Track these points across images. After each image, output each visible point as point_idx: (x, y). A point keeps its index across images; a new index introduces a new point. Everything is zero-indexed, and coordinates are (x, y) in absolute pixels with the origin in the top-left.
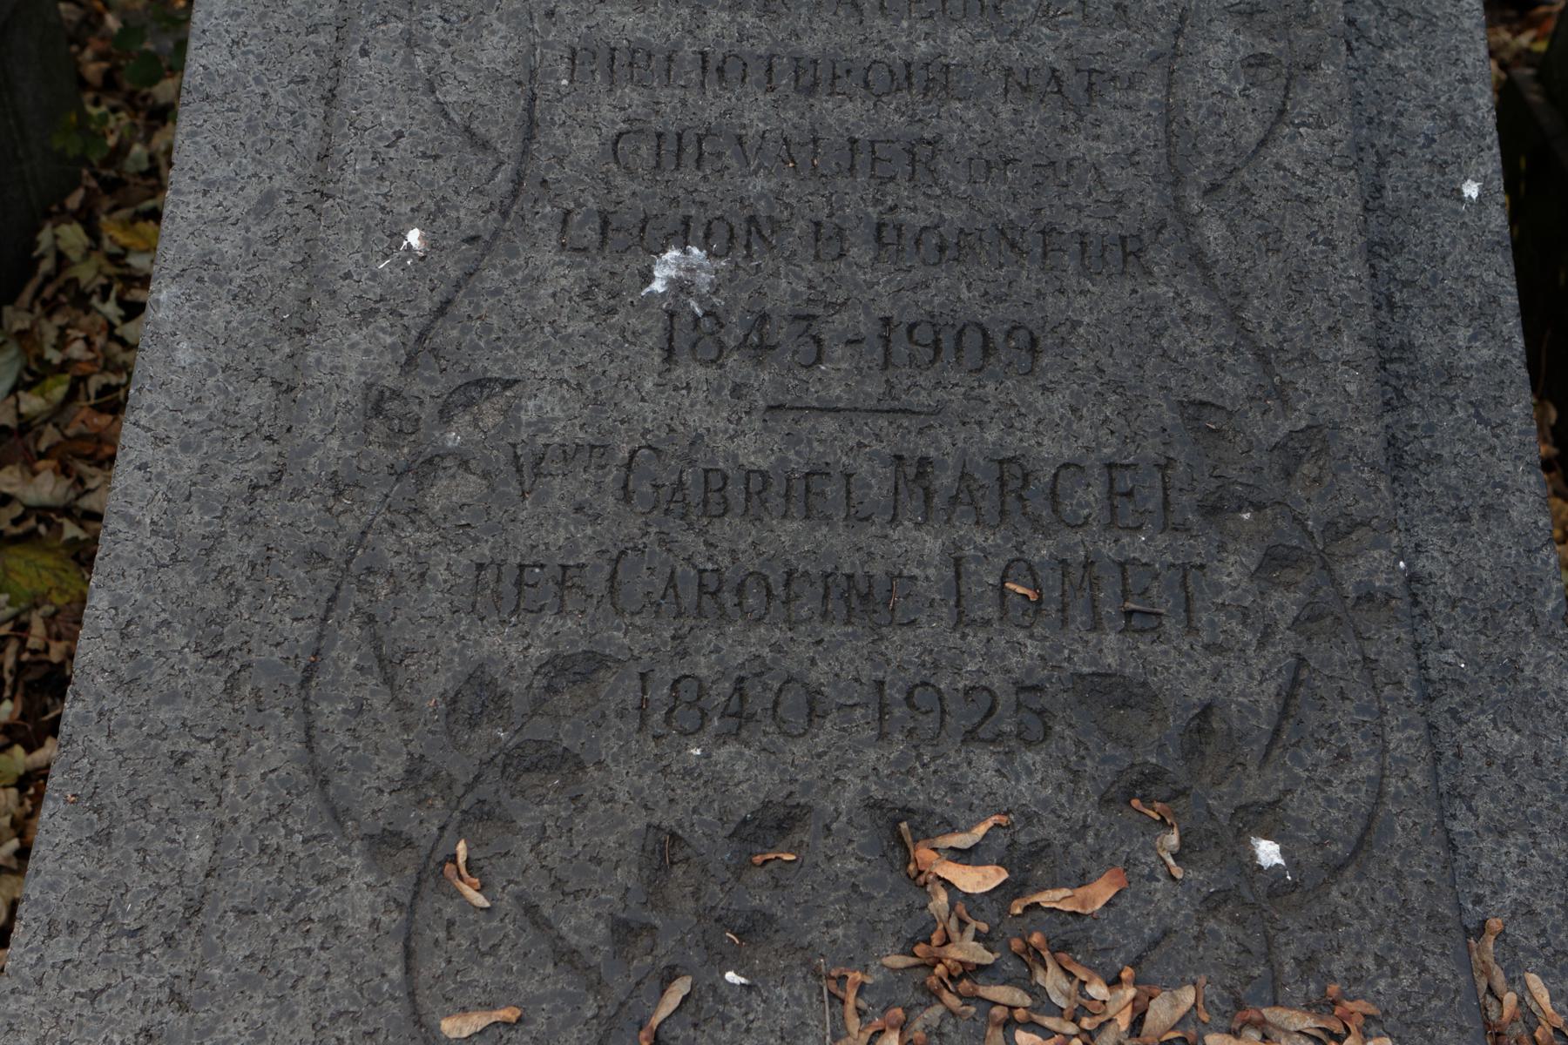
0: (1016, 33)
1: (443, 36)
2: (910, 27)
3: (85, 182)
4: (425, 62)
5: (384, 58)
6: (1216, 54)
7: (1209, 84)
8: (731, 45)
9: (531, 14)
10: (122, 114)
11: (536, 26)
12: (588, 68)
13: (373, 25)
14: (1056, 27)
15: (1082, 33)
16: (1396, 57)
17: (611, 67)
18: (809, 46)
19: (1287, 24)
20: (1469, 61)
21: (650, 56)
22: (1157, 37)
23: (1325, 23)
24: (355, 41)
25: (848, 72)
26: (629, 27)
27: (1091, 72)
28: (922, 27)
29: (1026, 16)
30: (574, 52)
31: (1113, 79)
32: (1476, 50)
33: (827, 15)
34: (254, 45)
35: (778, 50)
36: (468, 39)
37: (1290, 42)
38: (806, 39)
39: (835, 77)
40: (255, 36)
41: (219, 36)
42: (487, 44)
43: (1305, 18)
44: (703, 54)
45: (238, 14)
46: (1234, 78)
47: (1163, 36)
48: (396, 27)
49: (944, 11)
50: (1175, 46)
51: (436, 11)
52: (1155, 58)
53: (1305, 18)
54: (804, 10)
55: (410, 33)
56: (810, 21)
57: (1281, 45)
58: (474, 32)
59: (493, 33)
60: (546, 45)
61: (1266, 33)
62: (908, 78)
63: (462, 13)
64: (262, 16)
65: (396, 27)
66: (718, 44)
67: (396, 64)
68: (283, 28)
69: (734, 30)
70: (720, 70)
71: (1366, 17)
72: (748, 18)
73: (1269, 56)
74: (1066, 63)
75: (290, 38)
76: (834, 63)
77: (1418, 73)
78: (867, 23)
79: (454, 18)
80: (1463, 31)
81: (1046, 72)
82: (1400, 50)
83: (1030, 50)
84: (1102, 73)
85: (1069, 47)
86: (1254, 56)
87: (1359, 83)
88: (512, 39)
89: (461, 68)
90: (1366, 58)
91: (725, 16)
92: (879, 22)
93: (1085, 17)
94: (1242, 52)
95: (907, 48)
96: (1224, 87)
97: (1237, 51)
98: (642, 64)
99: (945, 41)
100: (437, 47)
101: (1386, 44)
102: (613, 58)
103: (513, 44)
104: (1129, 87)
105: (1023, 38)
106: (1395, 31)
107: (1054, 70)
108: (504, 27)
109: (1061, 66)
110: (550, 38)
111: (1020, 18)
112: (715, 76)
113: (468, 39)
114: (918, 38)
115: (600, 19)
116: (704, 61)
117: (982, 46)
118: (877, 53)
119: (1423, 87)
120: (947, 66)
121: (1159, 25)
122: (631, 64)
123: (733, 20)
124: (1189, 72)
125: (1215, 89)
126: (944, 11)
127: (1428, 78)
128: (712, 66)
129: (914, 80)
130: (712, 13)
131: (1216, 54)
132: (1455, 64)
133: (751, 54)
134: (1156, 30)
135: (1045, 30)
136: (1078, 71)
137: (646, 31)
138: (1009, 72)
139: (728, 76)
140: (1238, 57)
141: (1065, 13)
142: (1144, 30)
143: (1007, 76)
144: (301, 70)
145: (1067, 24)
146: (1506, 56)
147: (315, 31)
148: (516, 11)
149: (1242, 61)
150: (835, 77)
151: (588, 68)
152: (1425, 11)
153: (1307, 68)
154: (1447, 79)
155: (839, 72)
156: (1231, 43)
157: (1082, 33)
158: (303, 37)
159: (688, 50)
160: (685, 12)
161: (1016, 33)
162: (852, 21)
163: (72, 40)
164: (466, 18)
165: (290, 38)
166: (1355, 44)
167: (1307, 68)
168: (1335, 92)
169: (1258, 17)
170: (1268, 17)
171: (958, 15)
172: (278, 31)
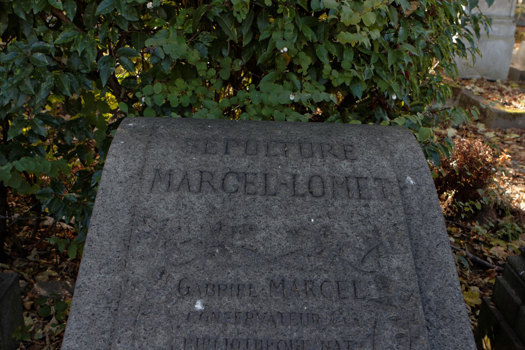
0: (324, 329)
1: (144, 335)
2: (291, 328)
3: (20, 346)
4: (138, 345)
5: (125, 344)
6: (387, 334)
7: (386, 345)
8: (235, 336)
9: (172, 327)
10: (36, 319)
11: (174, 331)
12: (190, 345)
13: (122, 332)
14: (337, 327)
15: (345, 328)
16: (443, 332)
17: (197, 344)
18: (260, 336)
19: (408, 323)
20: (466, 332)
21: (209, 341)
22: (368, 329)
23: (420, 323)
24: (116, 338)
25: (272, 344)
26: (203, 331)
27: (349, 341)
28: (295, 328)
29: (327, 323)
30: (185, 340)
31: (356, 344)
32: (468, 329)
33: (265, 325)
34: (84, 339)
35: (250, 337)
36: (152, 336)
37: (410, 329)
38: (258, 333)
39: (268, 346)
40: (85, 335)
41: (73, 336)
42: (158, 338)
43: (413, 321)
44: (226, 339)
45: (80, 328)
46: (394, 342)
47: (370, 329)
48: (130, 333)
49: (301, 322)
50: (374, 332)
51: (143, 327)
52: (368, 336)
53: (413, 321)
54: (258, 324)
55: (134, 335)
56: (260, 327)
57: (407, 330)
58: (154, 334)
59: (160, 334)
60: (177, 338)
61: (402, 326)
62: (291, 345)
63: (151, 328)
64: (88, 329)
65: (130, 333)
66: (231, 336)
67: (129, 345)
68: (94, 333)
69: (236, 331)
70: (232, 345)
71: (432, 319)
72: (240, 327)
73: (404, 334)
74: (341, 339)
75: (96, 336)
76: (267, 341)
77: (451, 337)
78: (278, 327)
79: (148, 329)
80: (463, 322)
81: (334, 342)
82: (444, 329)
83: (329, 335)
84: (352, 342)
85: (341, 333)
86: (399, 334)
87: (433, 341)
88: (166, 336)
89: (150, 346)
90: (434, 332)
91: (233, 326)
92: (281, 327)
93: (345, 323)
94: (395, 333)
95: (290, 335)
96: (391, 346)
97: (394, 333)
98: (207, 343)
99: (302, 333)
100: (142, 339)
101: (440, 327)
102: (198, 342)
103: (166, 338)
104: (361, 346)
105: (326, 331)
106: (442, 323)
107: (337, 341)
108: (163, 332)
109: (339, 340)
110: (178, 335)
111: (325, 324)
112: (230, 347)
113: (152, 336)
114: (294, 332)
115: (194, 328)
116: (227, 342)
117: (314, 334)
118: (281, 337)
119: (453, 341)
120: (303, 341)
121: (369, 325)
122: (203, 344)
123: (236, 328)
124: (380, 341)
125: (388, 346)
126: (301, 322)
127: (454, 338)
128: (229, 343)
129: (293, 346)
130: (229, 325)
131: (387, 334)
132: (462, 333)
133: (242, 339)
134: (368, 327)
135: (333, 328)
136: (344, 341)
137: (208, 332)
138: (323, 342)
139: (234, 347)
140: (394, 335)
141: (339, 322)
142: (364, 327)
143: (322, 344)
144: (98, 347)
145: (340, 325)
146: (482, 286)
147: (104, 333)
148: (168, 327)
149: (395, 336)
150: (268, 346)
151: (190, 345)
152: (450, 316)
153: (416, 338)
154: (460, 339)
155: (269, 344)
156: (391, 330)
157: (345, 328)
158: (100, 335)
159: (221, 338)
160: (221, 325)
161: (324, 329)
162: (273, 327)
163: (22, 294)
164: (152, 329)
165: (96, 336)
166: (430, 328)
167: (416, 338)
168: (426, 346)
169: (399, 321)
170: (402, 321)
171: (306, 324)
172: (92, 334)
